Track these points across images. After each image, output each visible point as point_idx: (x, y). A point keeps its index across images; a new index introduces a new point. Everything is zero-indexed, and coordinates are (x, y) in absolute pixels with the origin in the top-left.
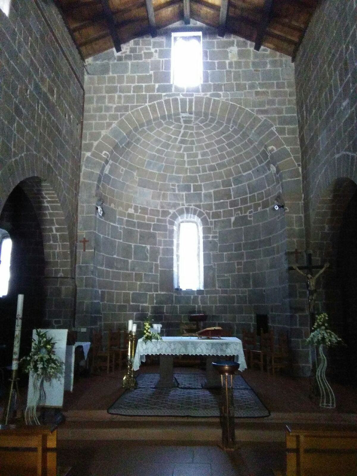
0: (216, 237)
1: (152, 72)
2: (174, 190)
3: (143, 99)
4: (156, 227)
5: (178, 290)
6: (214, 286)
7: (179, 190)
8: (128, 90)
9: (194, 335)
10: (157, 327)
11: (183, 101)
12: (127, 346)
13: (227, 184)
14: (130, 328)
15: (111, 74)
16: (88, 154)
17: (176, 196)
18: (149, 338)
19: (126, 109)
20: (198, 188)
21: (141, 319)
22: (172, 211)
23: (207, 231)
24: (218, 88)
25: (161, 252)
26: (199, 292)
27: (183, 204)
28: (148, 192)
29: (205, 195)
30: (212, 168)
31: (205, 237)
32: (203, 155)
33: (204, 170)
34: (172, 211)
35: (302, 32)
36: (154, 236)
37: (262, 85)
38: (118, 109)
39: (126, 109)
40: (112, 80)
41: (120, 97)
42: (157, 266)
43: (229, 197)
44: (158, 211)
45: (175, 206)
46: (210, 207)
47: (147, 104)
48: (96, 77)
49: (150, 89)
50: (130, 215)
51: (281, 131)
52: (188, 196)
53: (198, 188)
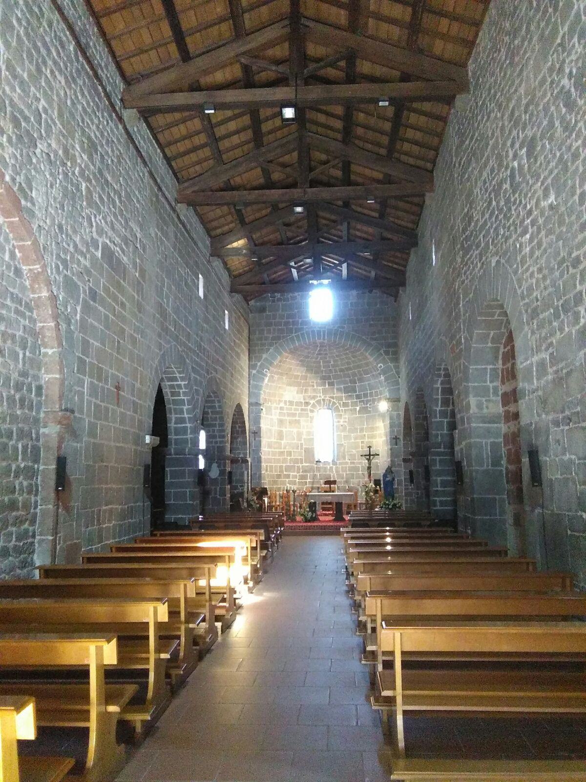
0: (345, 422)
2: (313, 386)
5: (334, 322)
6: (344, 459)
7: (317, 386)
9: (50, 668)
17: (314, 390)
22: (312, 402)
25: (304, 433)
41: (274, 330)
42: (302, 444)
44: (301, 403)
45: (314, 397)
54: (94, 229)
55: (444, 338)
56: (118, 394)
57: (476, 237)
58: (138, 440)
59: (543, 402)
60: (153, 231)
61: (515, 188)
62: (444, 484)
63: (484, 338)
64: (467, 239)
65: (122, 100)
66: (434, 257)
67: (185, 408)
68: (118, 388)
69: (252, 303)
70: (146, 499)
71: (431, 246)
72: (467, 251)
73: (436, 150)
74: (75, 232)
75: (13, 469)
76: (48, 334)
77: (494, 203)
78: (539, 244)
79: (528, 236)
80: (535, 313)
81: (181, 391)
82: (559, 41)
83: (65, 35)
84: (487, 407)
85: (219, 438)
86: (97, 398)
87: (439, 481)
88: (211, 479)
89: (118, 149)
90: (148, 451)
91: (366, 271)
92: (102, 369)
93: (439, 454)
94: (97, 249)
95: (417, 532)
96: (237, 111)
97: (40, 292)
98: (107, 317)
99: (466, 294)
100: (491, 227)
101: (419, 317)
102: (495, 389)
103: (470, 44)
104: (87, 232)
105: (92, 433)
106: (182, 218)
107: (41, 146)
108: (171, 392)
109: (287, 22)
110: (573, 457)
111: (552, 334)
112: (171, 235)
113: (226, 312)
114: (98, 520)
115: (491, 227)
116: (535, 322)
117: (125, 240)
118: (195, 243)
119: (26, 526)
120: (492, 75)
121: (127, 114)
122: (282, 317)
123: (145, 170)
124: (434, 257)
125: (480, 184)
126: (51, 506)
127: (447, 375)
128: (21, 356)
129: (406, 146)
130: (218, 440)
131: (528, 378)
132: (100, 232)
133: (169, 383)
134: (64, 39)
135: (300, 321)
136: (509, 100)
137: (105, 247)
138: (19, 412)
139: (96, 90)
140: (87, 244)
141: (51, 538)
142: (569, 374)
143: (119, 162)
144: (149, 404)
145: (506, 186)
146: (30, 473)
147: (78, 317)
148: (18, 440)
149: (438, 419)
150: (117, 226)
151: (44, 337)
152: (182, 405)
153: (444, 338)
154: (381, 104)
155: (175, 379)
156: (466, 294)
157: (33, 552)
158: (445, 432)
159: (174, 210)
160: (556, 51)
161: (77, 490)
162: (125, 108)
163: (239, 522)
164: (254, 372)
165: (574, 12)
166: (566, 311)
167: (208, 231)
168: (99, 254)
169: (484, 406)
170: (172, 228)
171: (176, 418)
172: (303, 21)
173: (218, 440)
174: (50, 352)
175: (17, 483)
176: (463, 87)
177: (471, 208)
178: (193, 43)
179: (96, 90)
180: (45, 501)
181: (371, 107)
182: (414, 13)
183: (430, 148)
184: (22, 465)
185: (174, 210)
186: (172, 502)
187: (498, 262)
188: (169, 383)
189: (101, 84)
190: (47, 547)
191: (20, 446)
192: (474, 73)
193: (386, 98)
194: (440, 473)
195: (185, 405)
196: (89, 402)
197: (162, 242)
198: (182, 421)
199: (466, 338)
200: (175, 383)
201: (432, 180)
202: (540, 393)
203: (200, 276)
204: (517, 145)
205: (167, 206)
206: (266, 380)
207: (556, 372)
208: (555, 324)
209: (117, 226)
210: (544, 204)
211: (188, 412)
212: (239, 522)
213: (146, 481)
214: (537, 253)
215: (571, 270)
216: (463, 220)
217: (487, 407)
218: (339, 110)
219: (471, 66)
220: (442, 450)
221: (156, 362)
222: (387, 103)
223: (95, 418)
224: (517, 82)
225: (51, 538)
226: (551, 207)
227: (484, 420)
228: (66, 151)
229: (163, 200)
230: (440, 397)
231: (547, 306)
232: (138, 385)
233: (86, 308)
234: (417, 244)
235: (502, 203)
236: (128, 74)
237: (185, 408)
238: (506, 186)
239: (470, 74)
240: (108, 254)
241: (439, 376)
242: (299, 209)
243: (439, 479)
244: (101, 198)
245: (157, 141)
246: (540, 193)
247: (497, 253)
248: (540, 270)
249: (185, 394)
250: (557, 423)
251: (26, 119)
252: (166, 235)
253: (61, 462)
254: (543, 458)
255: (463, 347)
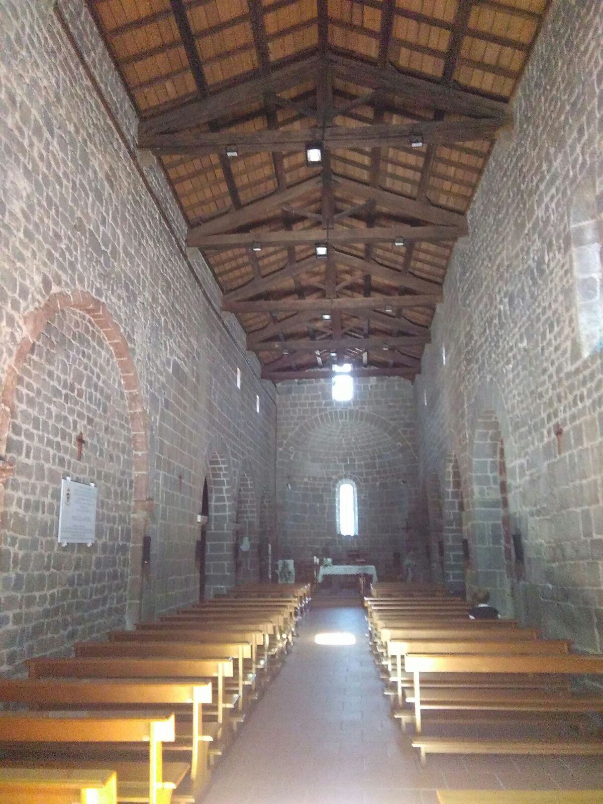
1: (320, 393)
2: (335, 462)
3: (314, 411)
4: (323, 490)
5: (340, 535)
8: (304, 405)
10: (329, 560)
11: (341, 412)
13: (373, 458)
15: (293, 394)
16: (281, 449)
18: (326, 566)
19: (304, 418)
20: (352, 460)
23: (359, 492)
24: (363, 403)
26: (355, 536)
27: (343, 471)
29: (358, 465)
30: (362, 448)
31: (358, 497)
32: (356, 439)
33: (357, 448)
34: (334, 477)
35: (486, 156)
36: (321, 496)
37: (392, 401)
38: (299, 418)
39: (304, 418)
40: (294, 398)
41: (299, 410)
43: (375, 468)
45: (336, 473)
46: (361, 474)
48: (284, 396)
49: (319, 404)
50: (306, 483)
51: (405, 432)
53: (352, 460)
54: (168, 351)
55: (453, 430)
56: (181, 482)
57: (476, 353)
58: (192, 520)
59: (524, 496)
60: (205, 340)
61: (502, 324)
62: (457, 558)
63: (484, 436)
64: (468, 352)
65: (186, 241)
66: (444, 358)
68: (180, 477)
71: (441, 346)
72: (469, 362)
73: (445, 268)
74: (157, 356)
76: (139, 440)
77: (488, 331)
78: (518, 375)
79: (511, 366)
80: (517, 427)
81: (222, 473)
82: (526, 232)
83: (154, 208)
84: (488, 494)
86: (48, 433)
88: (242, 551)
89: (183, 281)
90: (198, 528)
92: (171, 462)
94: (169, 366)
95: (432, 601)
96: (277, 248)
97: (136, 408)
98: (174, 419)
99: (469, 399)
100: (486, 350)
102: (495, 478)
103: (469, 199)
104: (165, 355)
105: (164, 517)
106: (225, 322)
107: (140, 299)
108: (213, 474)
109: (320, 178)
110: (543, 541)
111: (528, 446)
112: (217, 338)
115: (486, 350)
116: (517, 433)
117: (187, 354)
118: (235, 342)
120: (485, 232)
121: (188, 251)
122: (307, 398)
123: (200, 291)
124: (444, 358)
125: (477, 312)
126: (138, 576)
127: (456, 461)
128: (122, 459)
129: (422, 256)
131: (513, 476)
132: (172, 352)
133: (212, 466)
134: (153, 211)
136: (496, 257)
137: (175, 364)
138: (120, 503)
139: (171, 241)
140: (164, 364)
141: (138, 602)
142: (539, 478)
143: (184, 291)
144: (200, 488)
145: (496, 321)
147: (158, 424)
148: (118, 525)
149: (450, 500)
150: (183, 344)
151: (136, 442)
153: (453, 430)
154: (397, 244)
155: (217, 463)
156: (469, 399)
157: (124, 613)
159: (220, 318)
160: (525, 237)
161: (154, 562)
162: (188, 246)
165: (535, 217)
166: (536, 430)
167: (244, 328)
168: (171, 371)
170: (218, 334)
172: (334, 177)
174: (140, 453)
176: (463, 231)
177: (471, 328)
178: (243, 197)
179: (171, 241)
181: (389, 245)
182: (422, 177)
183: (440, 267)
184: (121, 544)
185: (220, 318)
186: (212, 573)
187: (491, 379)
188: (212, 466)
189: (175, 237)
191: (120, 528)
192: (472, 223)
193: (401, 240)
194: (452, 548)
196: (163, 491)
197: (211, 347)
198: (222, 499)
199: (469, 435)
200: (216, 466)
201: (441, 293)
202: (521, 489)
204: (502, 294)
205: (215, 315)
207: (531, 475)
208: (529, 438)
209: (183, 344)
210: (521, 345)
213: (197, 552)
214: (517, 381)
215: (538, 401)
216: (466, 336)
217: (488, 494)
218: (361, 246)
219: (469, 216)
220: (454, 527)
222: (402, 244)
223: (166, 504)
224: (501, 246)
226: (525, 350)
227: (485, 504)
228: (153, 298)
229: (211, 311)
231: (524, 424)
233: (163, 416)
234: (430, 339)
235: (493, 333)
236: (190, 219)
238: (496, 321)
239: (469, 222)
240: (177, 367)
241: (450, 461)
242: (327, 317)
243: (452, 553)
244: (173, 326)
245: (208, 263)
246: (517, 336)
247: (490, 372)
248: (519, 394)
249: (225, 475)
250: (532, 515)
251: (133, 283)
252: (213, 340)
253: (147, 541)
254: (525, 541)
255: (467, 441)
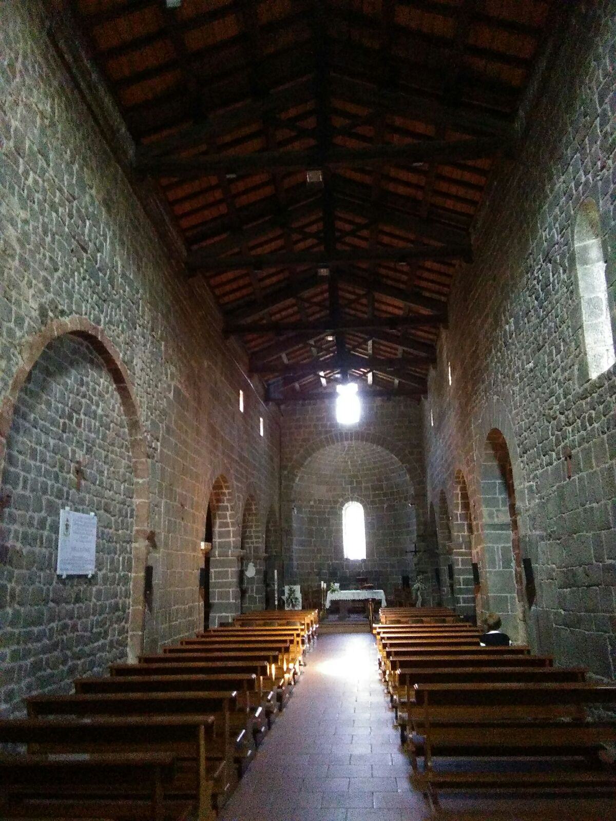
5: (360, 425)
12: (351, 586)
13: (379, 480)
14: (322, 586)
18: (334, 591)
21: (328, 582)
22: (341, 500)
26: (363, 561)
28: (323, 488)
40: (298, 420)
47: (322, 437)
50: (312, 507)
52: (352, 489)
67: (228, 513)
69: (282, 407)
70: (201, 599)
75: (117, 577)
84: (497, 517)
85: (256, 538)
87: (461, 581)
91: (391, 378)
93: (461, 554)
101: (440, 423)
113: (241, 392)
114: (169, 620)
119: (123, 624)
124: (450, 378)
126: (141, 608)
130: (254, 540)
135: (329, 423)
141: (140, 633)
146: (125, 580)
149: (459, 522)
152: (224, 511)
158: (466, 533)
163: (444, 616)
164: (286, 472)
168: (171, 396)
169: (495, 515)
171: (220, 522)
173: (254, 540)
175: (118, 588)
180: (135, 602)
186: (216, 601)
190: (137, 641)
191: (121, 559)
194: (463, 572)
195: (228, 511)
198: (226, 525)
203: (241, 392)
206: (297, 479)
211: (232, 516)
212: (444, 616)
217: (497, 517)
221: (209, 476)
225: (140, 633)
230: (460, 502)
232: (196, 499)
237: (228, 513)
247: (497, 393)
250: (542, 538)
253: (149, 571)
